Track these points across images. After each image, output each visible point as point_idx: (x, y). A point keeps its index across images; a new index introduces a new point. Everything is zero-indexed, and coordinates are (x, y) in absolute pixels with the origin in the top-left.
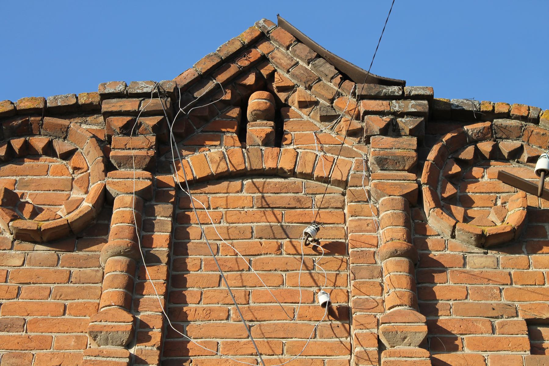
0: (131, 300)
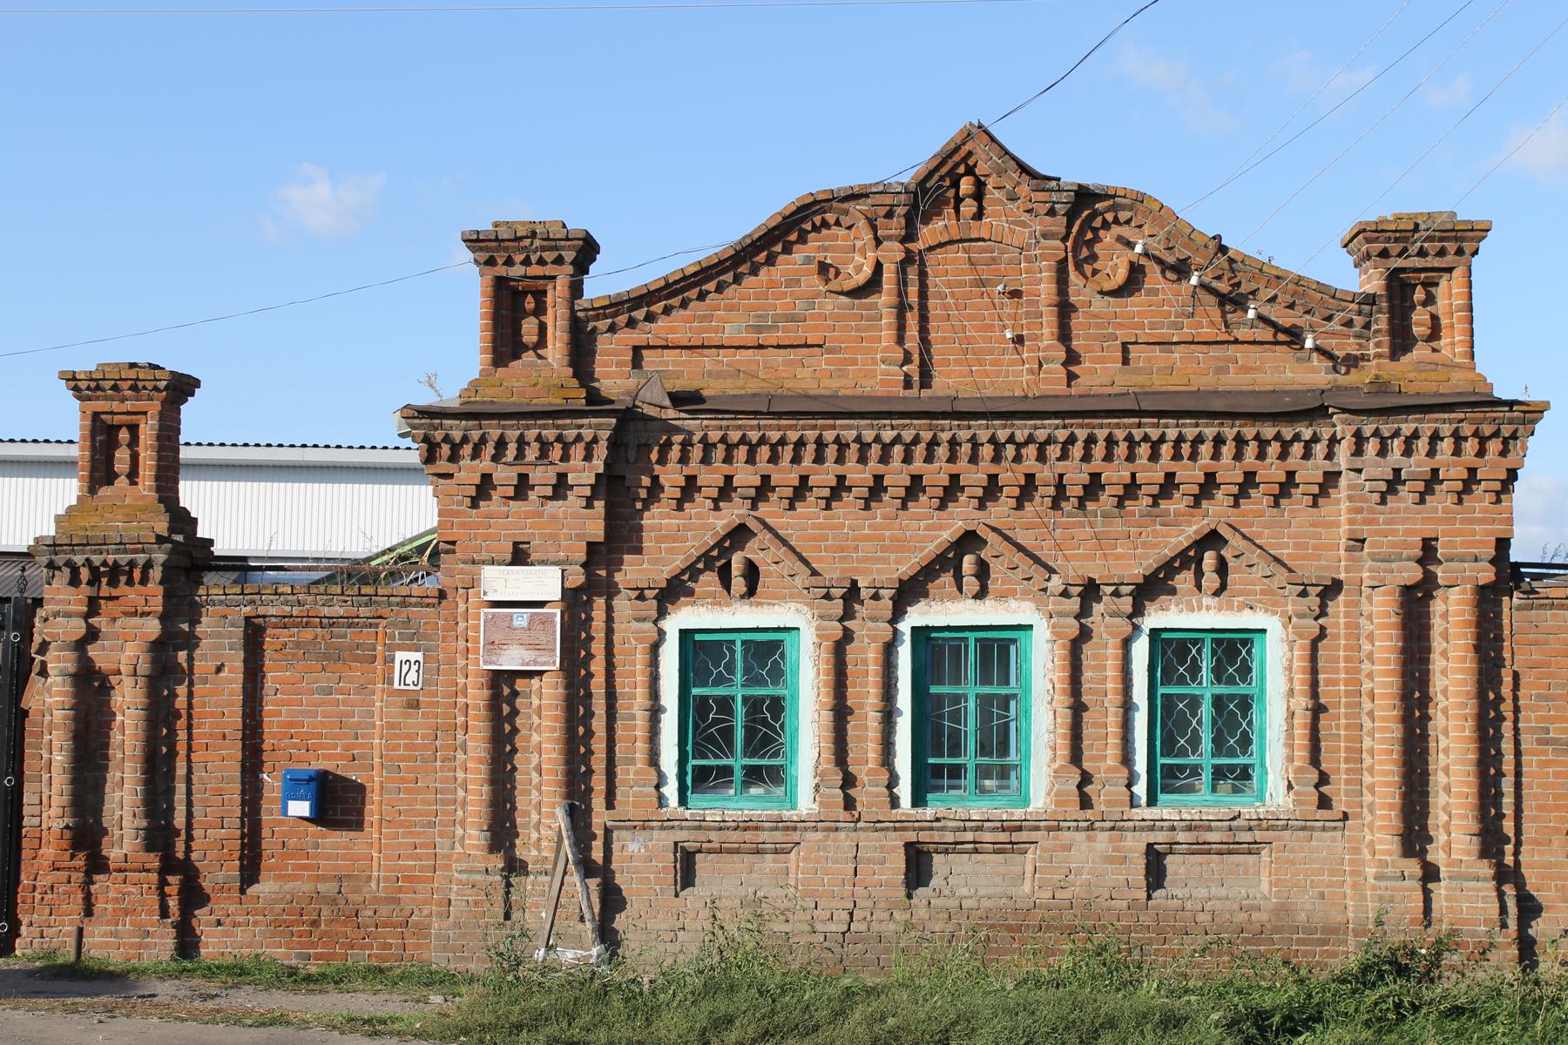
0: (900, 340)
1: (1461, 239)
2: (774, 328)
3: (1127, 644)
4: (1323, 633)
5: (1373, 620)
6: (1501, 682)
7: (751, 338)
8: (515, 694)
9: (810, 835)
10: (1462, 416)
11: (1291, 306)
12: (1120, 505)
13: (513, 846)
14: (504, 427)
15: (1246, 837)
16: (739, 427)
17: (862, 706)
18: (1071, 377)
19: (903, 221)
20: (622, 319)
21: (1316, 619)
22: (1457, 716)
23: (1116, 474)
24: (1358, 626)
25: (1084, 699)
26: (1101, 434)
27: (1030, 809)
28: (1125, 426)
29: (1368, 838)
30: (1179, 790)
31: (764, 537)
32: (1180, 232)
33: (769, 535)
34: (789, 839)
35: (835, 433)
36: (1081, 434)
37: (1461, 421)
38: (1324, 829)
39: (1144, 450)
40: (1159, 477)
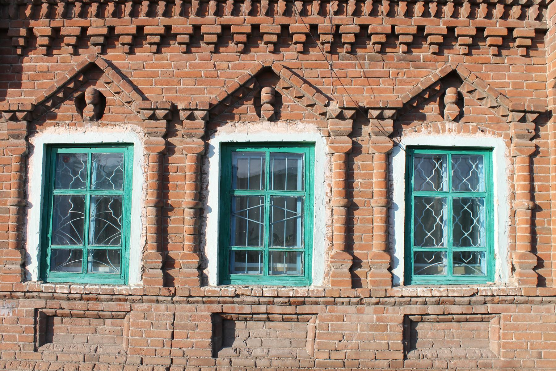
3: (389, 156)
25: (356, 200)
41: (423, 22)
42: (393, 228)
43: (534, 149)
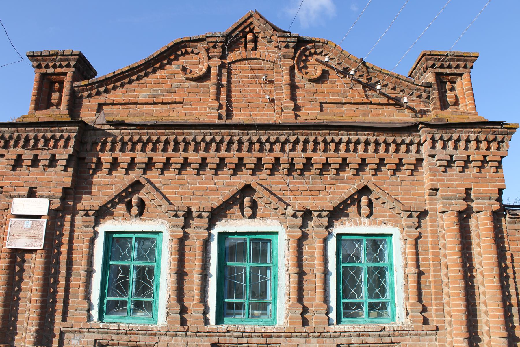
0: (218, 99)
1: (466, 60)
2: (162, 95)
3: (325, 241)
4: (420, 237)
5: (443, 229)
6: (506, 259)
7: (150, 100)
8: (24, 261)
9: (163, 338)
10: (480, 130)
11: (394, 89)
12: (321, 174)
13: (13, 340)
14: (28, 131)
15: (387, 340)
16: (138, 134)
17: (192, 272)
18: (297, 116)
19: (221, 49)
20: (94, 92)
21: (416, 229)
22: (489, 276)
23: (318, 158)
24: (437, 231)
25: (304, 269)
26: (311, 138)
27: (276, 326)
28: (323, 135)
29: (449, 339)
30: (352, 316)
31: (148, 187)
32: (342, 55)
33: (150, 186)
34: (152, 340)
35: (183, 137)
36: (302, 138)
37: (479, 132)
38: (426, 335)
39: (332, 147)
40: (340, 160)
41: (346, 155)
42: (329, 287)
43: (418, 235)
